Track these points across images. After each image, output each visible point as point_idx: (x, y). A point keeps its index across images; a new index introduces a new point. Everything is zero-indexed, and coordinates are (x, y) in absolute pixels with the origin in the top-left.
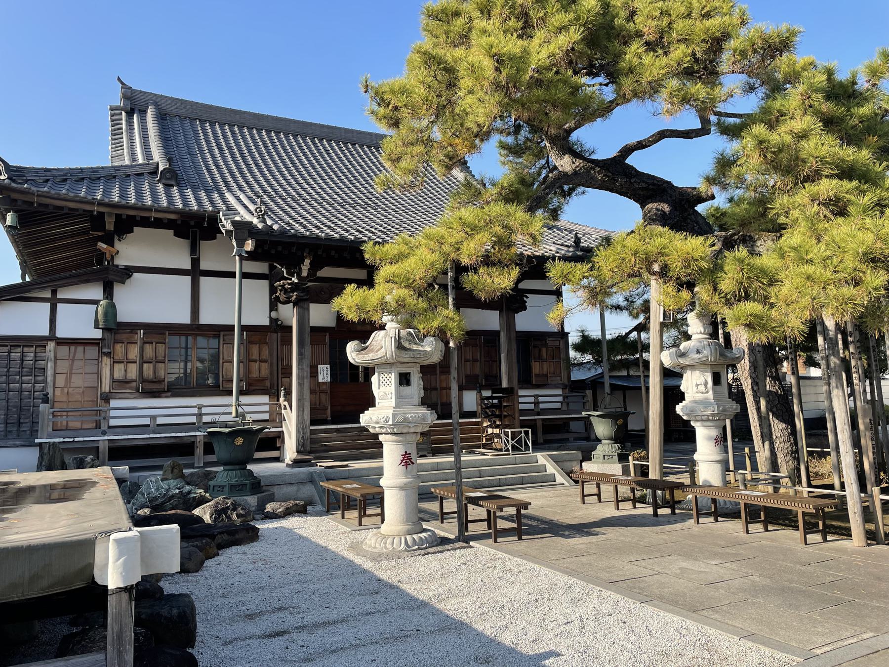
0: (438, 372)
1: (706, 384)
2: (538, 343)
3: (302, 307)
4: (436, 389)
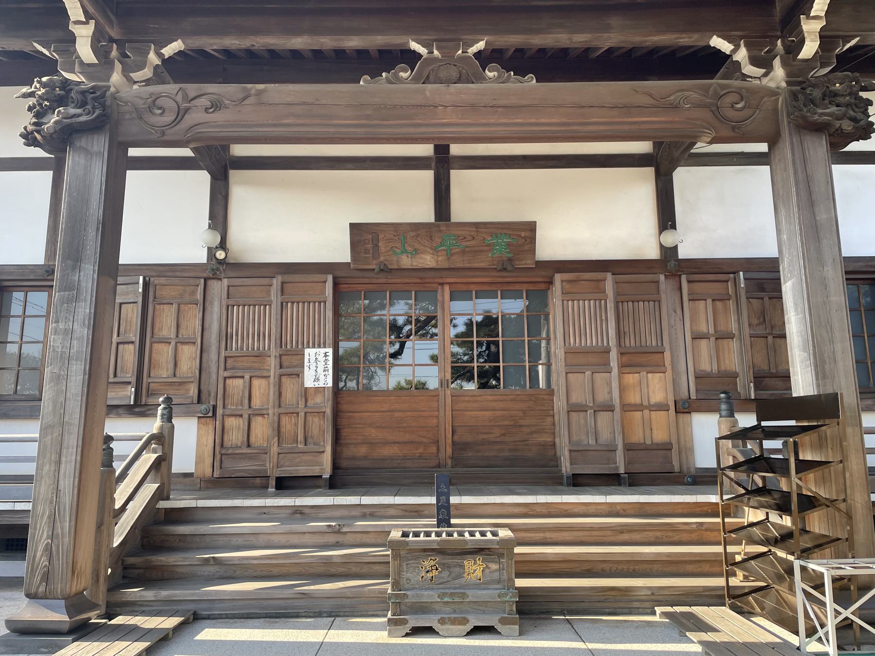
0: (614, 364)
3: (87, 151)
4: (610, 408)
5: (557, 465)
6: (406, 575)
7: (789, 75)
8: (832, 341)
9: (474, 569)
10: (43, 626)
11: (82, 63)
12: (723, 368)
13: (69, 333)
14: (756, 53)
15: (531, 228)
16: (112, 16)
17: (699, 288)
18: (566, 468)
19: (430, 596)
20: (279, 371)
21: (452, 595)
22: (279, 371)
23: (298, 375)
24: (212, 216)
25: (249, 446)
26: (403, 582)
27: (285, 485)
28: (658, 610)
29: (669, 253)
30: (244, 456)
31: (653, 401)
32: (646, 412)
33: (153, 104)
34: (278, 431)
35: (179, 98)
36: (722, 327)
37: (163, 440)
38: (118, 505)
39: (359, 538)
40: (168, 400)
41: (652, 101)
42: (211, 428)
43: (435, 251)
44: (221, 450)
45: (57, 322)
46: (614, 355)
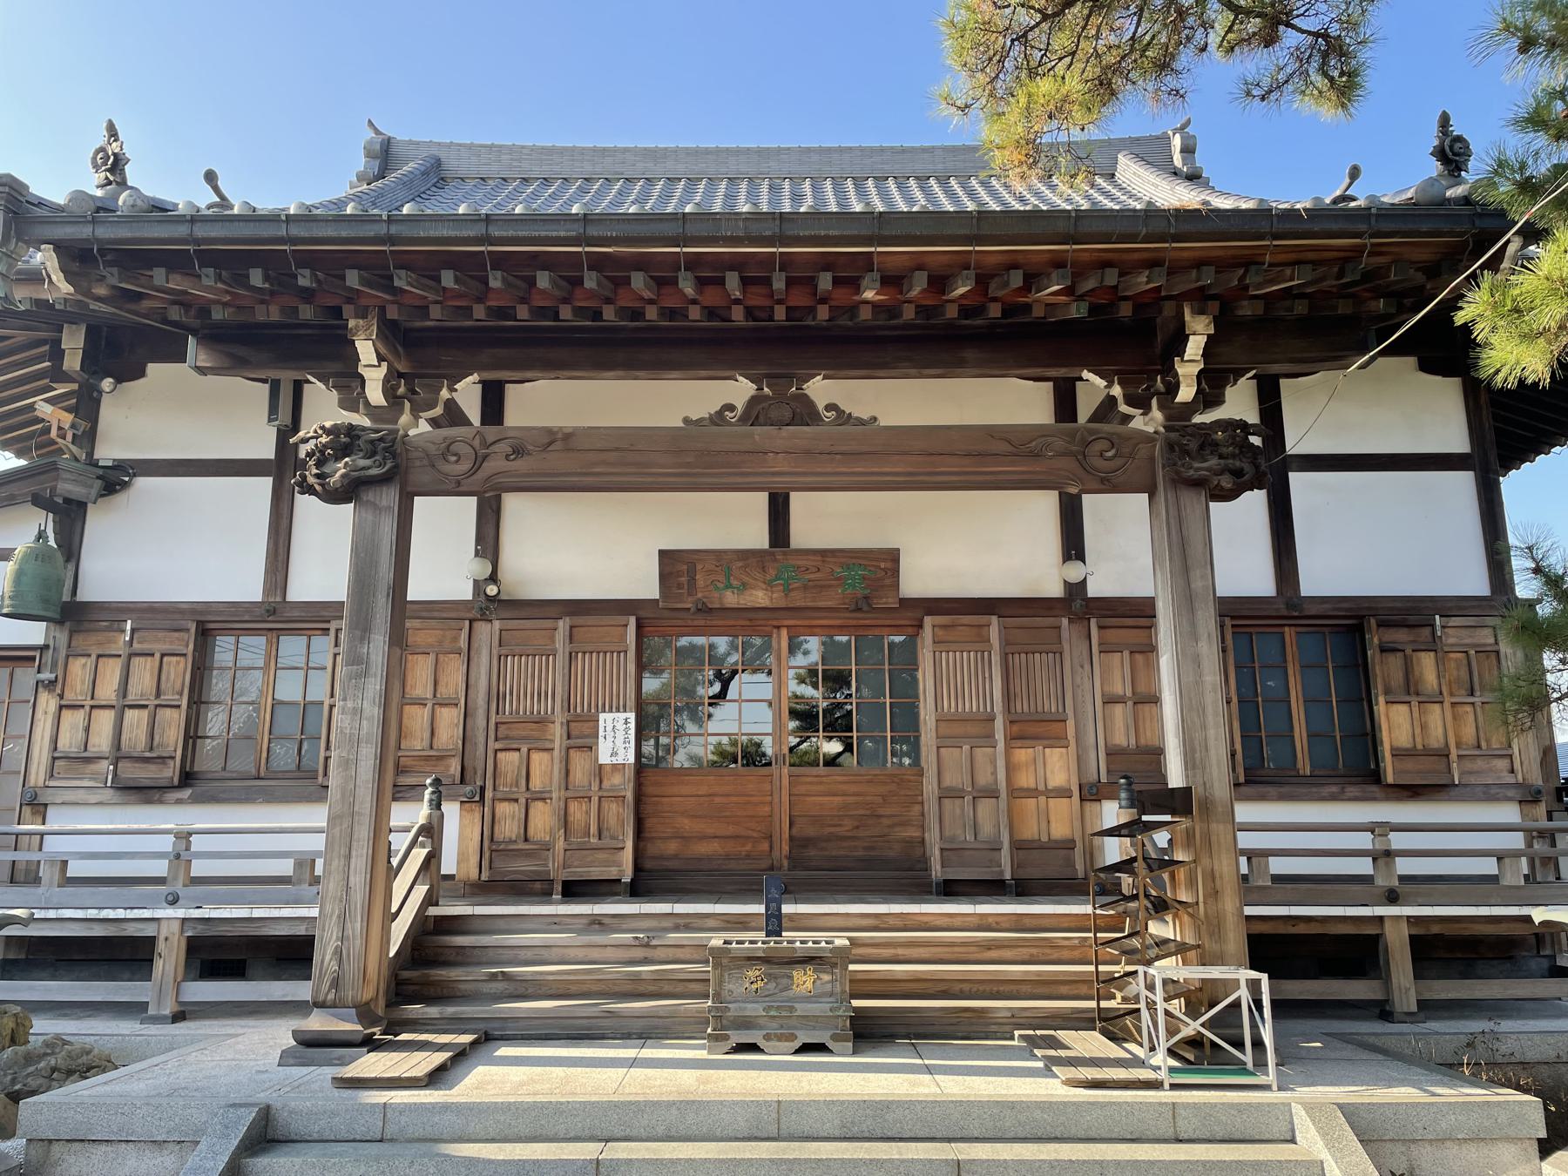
0: (1000, 736)
2: (1400, 636)
3: (375, 506)
4: (993, 794)
5: (927, 869)
6: (728, 986)
7: (1168, 418)
8: (1204, 727)
9: (804, 980)
10: (334, 1037)
11: (367, 403)
12: (1143, 742)
13: (358, 712)
14: (1131, 390)
15: (893, 556)
16: (400, 349)
17: (1112, 635)
18: (937, 872)
19: (755, 1009)
20: (566, 743)
21: (778, 1008)
22: (566, 743)
23: (591, 748)
24: (480, 539)
25: (526, 840)
26: (725, 993)
27: (574, 890)
28: (1017, 1033)
29: (1076, 590)
31: (1051, 785)
32: (1042, 799)
33: (447, 450)
34: (566, 823)
35: (476, 443)
36: (1141, 688)
37: (431, 831)
38: (394, 910)
39: (671, 953)
40: (437, 782)
41: (1011, 449)
42: (478, 816)
43: (769, 585)
44: (491, 846)
45: (345, 699)
46: (999, 724)
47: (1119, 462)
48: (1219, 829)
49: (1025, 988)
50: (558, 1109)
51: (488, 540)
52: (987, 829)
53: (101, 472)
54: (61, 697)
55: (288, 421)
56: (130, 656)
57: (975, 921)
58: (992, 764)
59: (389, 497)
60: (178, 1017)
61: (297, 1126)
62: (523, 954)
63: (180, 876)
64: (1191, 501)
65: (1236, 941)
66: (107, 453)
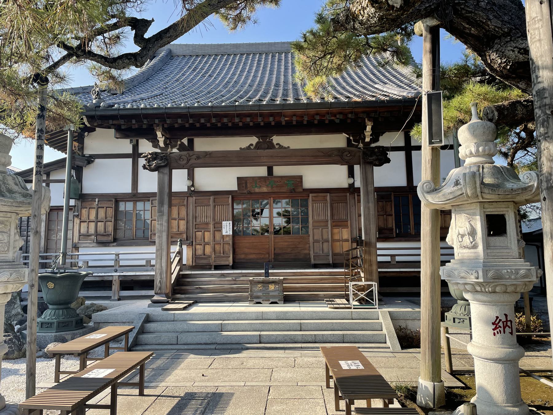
1: (473, 233)
3: (163, 173)
4: (327, 241)
5: (310, 261)
8: (370, 224)
9: (272, 287)
13: (162, 224)
15: (301, 177)
18: (313, 262)
19: (260, 294)
23: (220, 231)
27: (217, 268)
30: (202, 258)
31: (344, 238)
32: (341, 242)
33: (180, 157)
35: (187, 156)
37: (180, 253)
39: (241, 282)
40: (181, 241)
42: (191, 249)
43: (267, 186)
44: (195, 257)
47: (351, 157)
48: (373, 250)
49: (329, 289)
50: (213, 314)
51: (191, 176)
52: (326, 250)
53: (86, 158)
54: (80, 219)
55: (135, 143)
56: (98, 208)
57: (319, 274)
58: (327, 234)
59: (166, 170)
60: (119, 299)
61: (155, 318)
62: (204, 283)
63: (117, 266)
64: (368, 167)
65: (375, 276)
66: (88, 152)
